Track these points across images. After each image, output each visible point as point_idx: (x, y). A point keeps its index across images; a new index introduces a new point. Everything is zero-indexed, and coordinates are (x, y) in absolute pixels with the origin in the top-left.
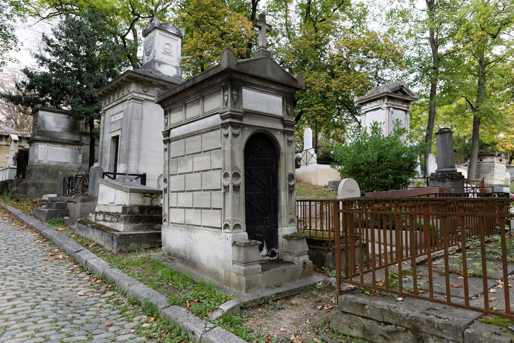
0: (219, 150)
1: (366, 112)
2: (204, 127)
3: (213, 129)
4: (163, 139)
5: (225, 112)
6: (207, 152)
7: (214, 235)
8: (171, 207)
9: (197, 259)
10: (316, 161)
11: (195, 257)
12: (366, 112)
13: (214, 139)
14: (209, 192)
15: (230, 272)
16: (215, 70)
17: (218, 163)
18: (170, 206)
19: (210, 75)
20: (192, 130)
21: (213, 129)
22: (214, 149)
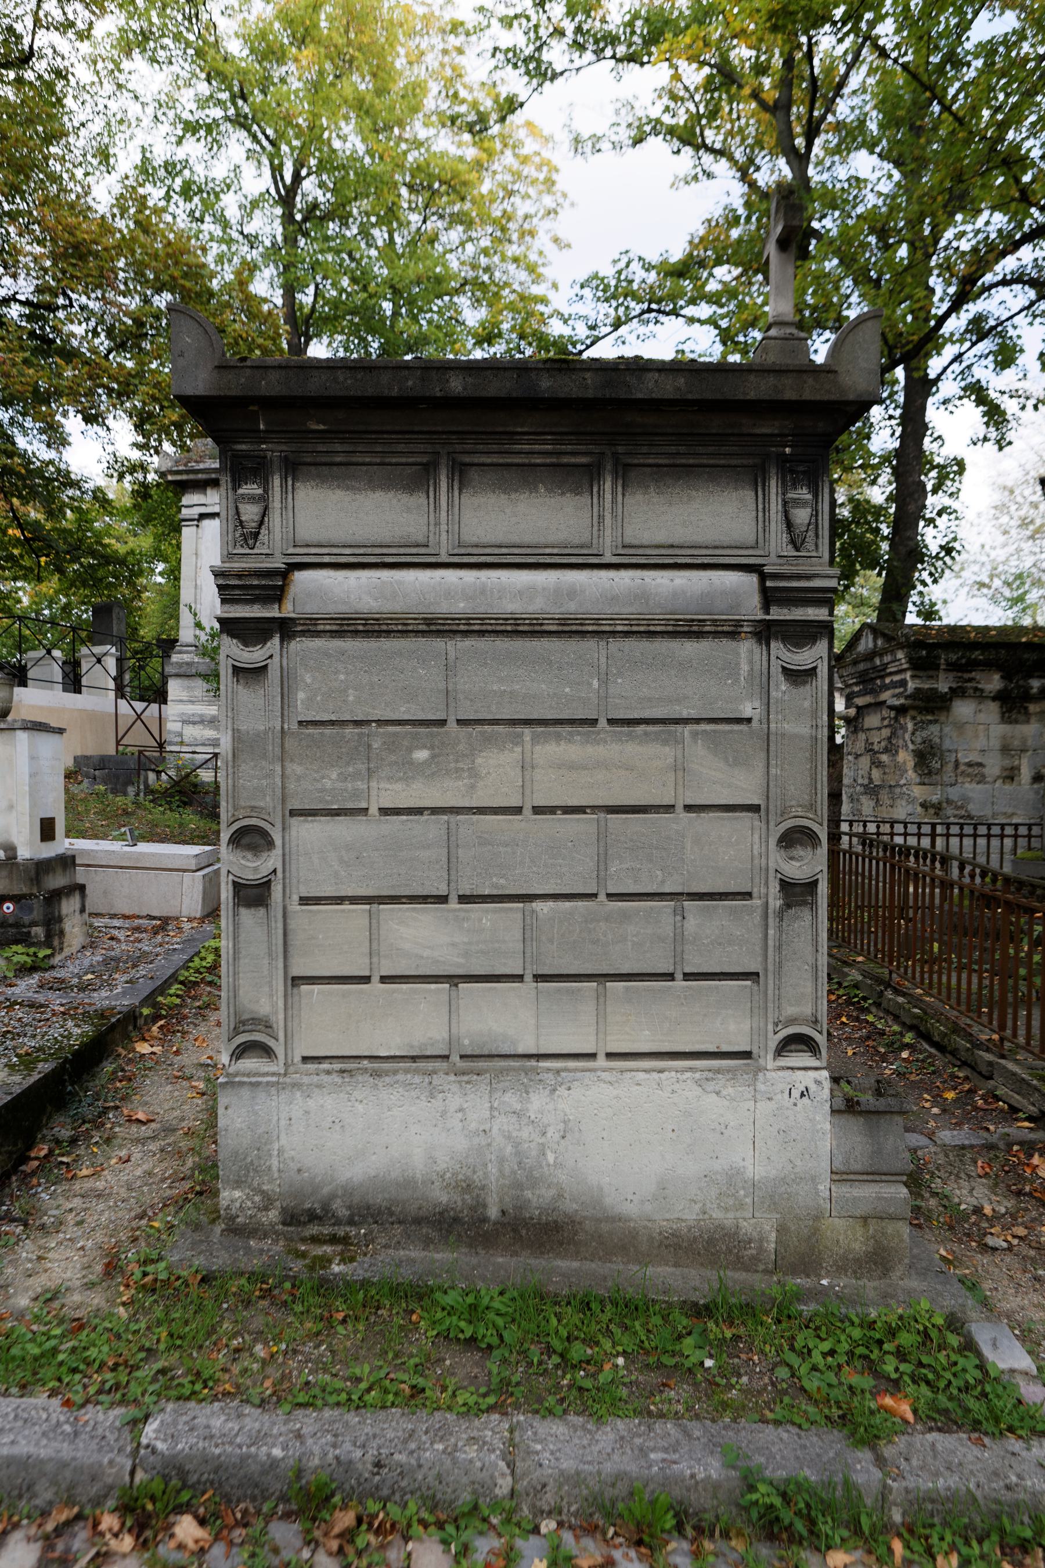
0: (743, 727)
1: (203, 516)
2: (609, 610)
3: (689, 628)
4: (218, 612)
5: (809, 577)
6: (641, 729)
7: (710, 1086)
8: (297, 981)
9: (569, 1206)
10: (154, 707)
11: (560, 1196)
12: (203, 516)
13: (733, 676)
14: (666, 906)
15: (817, 1218)
16: (788, 380)
17: (744, 785)
18: (296, 971)
19: (752, 395)
20: (511, 607)
21: (689, 628)
22: (698, 721)
